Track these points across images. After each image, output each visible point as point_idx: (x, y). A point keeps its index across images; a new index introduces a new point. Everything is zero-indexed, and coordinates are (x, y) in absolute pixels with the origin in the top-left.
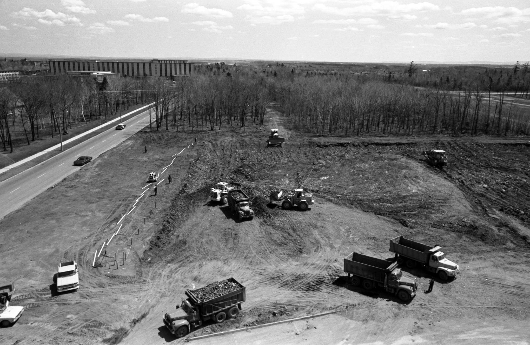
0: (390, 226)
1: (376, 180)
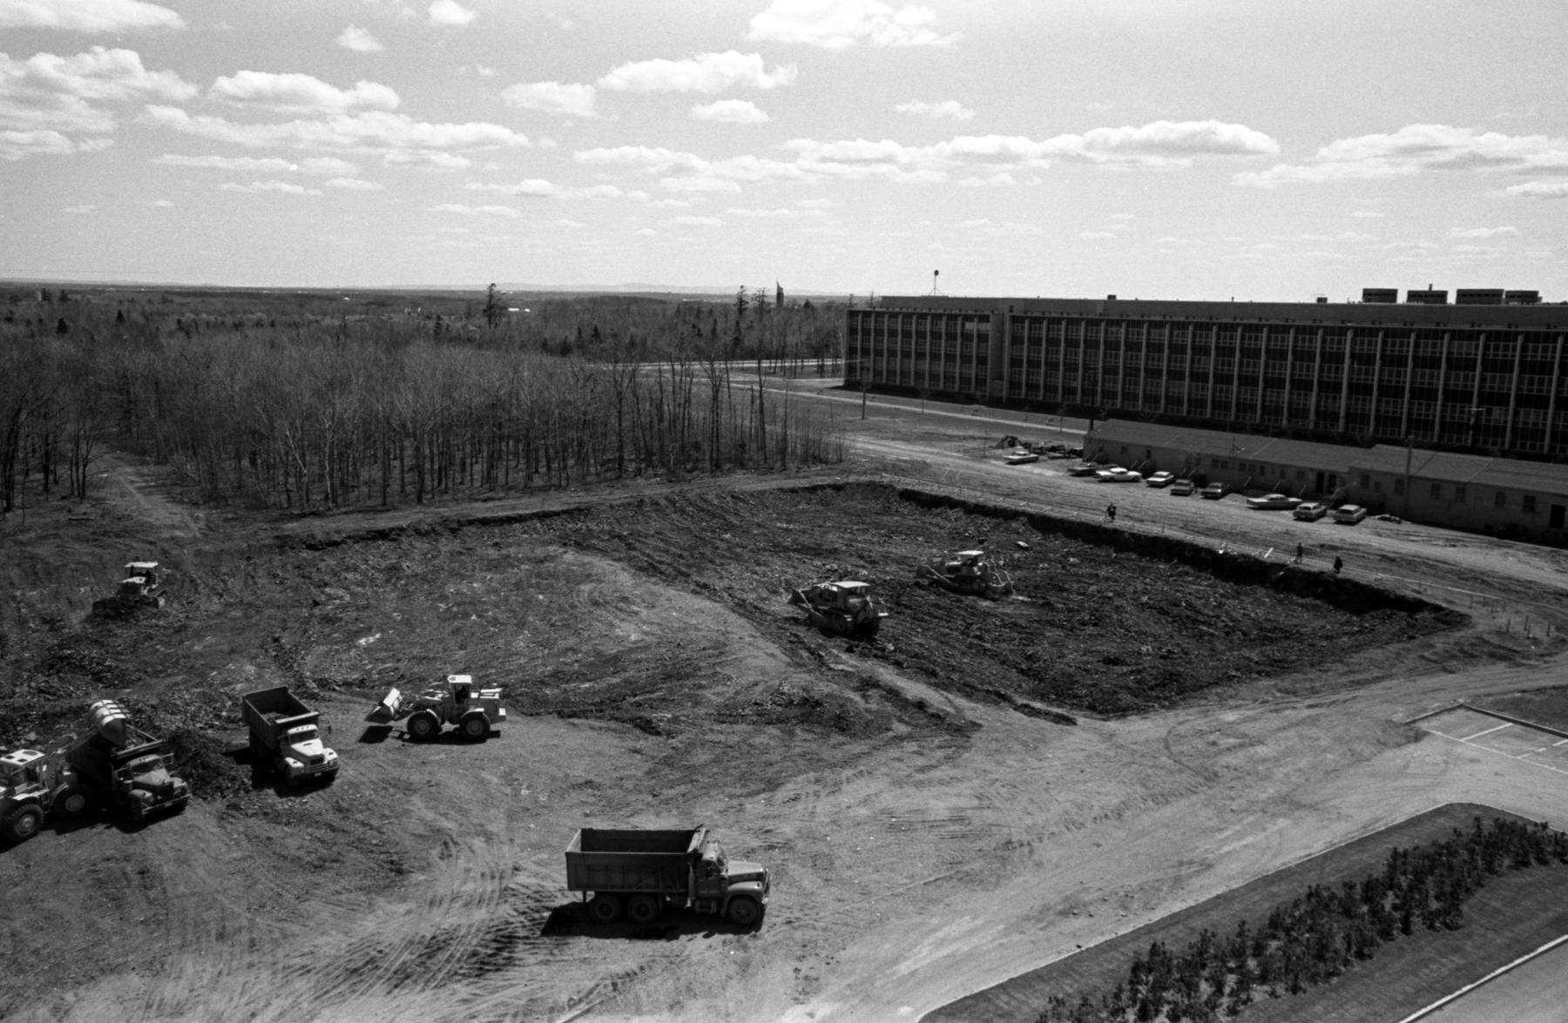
0: (615, 742)
1: (522, 625)
